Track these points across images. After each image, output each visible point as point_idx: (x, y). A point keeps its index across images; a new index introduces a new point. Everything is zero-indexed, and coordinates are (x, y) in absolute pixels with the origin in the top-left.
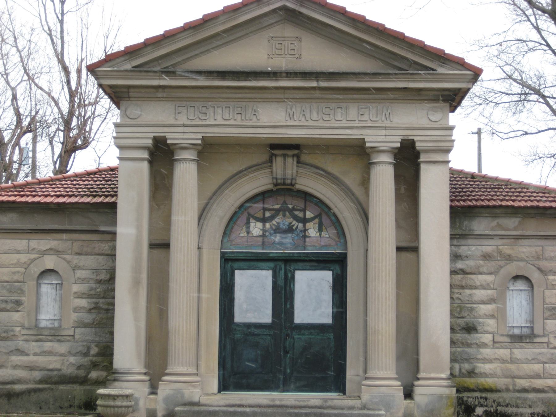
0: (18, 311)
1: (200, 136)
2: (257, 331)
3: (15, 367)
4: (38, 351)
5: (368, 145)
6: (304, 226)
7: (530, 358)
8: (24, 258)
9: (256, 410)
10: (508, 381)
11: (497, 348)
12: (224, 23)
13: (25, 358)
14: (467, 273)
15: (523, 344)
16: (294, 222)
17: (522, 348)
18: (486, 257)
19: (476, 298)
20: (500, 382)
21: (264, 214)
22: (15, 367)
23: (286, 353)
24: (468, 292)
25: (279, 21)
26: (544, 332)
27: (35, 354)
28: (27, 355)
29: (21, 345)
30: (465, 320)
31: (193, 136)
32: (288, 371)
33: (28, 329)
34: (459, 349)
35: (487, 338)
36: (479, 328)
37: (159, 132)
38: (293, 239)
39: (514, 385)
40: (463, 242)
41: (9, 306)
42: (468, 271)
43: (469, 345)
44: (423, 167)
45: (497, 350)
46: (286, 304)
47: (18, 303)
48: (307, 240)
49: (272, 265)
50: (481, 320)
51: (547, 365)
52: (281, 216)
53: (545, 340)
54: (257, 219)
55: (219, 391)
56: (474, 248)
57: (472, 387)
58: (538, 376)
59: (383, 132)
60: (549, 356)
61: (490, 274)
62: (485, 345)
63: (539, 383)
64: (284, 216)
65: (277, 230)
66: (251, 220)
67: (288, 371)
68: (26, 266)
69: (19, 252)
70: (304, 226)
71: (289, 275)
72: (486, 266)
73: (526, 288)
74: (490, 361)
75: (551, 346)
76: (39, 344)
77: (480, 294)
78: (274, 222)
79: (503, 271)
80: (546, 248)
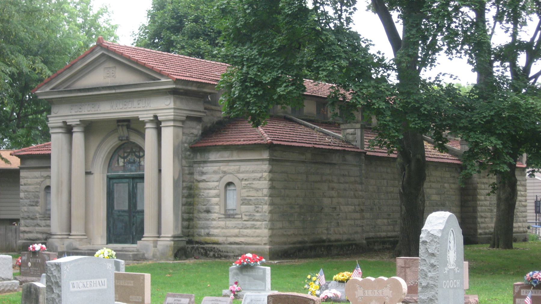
0: (37, 206)
1: (78, 120)
2: (123, 214)
3: (37, 232)
4: (44, 224)
5: (140, 119)
6: (140, 160)
7: (234, 226)
8: (39, 180)
9: (402, 284)
10: (224, 238)
11: (220, 221)
12: (80, 65)
13: (40, 228)
14: (207, 182)
15: (231, 219)
16: (136, 158)
17: (231, 221)
18: (215, 172)
19: (210, 195)
20: (220, 239)
21: (124, 155)
22: (37, 232)
23: (134, 224)
24: (207, 191)
25: (104, 61)
26: (232, 210)
27: (44, 226)
28: (41, 227)
29: (39, 222)
30: (206, 206)
31: (76, 120)
32: (134, 234)
33: (41, 214)
34: (203, 222)
35: (214, 216)
36: (211, 211)
37: (64, 119)
38: (135, 166)
39: (226, 240)
40: (206, 165)
41: (34, 204)
42: (207, 180)
43: (208, 220)
44: (163, 129)
45: (219, 222)
46: (133, 200)
47: (37, 202)
48: (141, 167)
49: (127, 180)
50: (213, 206)
51: (241, 230)
52: (130, 155)
53: (240, 216)
54: (122, 158)
55: (107, 244)
56: (209, 168)
57: (208, 242)
58: (236, 236)
59: (145, 112)
60: (241, 225)
61: (217, 181)
62: (214, 220)
63: (238, 240)
64: (132, 155)
65: (130, 163)
66: (120, 158)
67: (134, 234)
68: (40, 184)
69: (37, 178)
70: (140, 160)
71: (135, 185)
72: (216, 177)
73: (481, 191)
74: (217, 228)
75: (243, 220)
76: (45, 221)
77: (213, 192)
78: (128, 159)
79: (223, 180)
80: (242, 166)
